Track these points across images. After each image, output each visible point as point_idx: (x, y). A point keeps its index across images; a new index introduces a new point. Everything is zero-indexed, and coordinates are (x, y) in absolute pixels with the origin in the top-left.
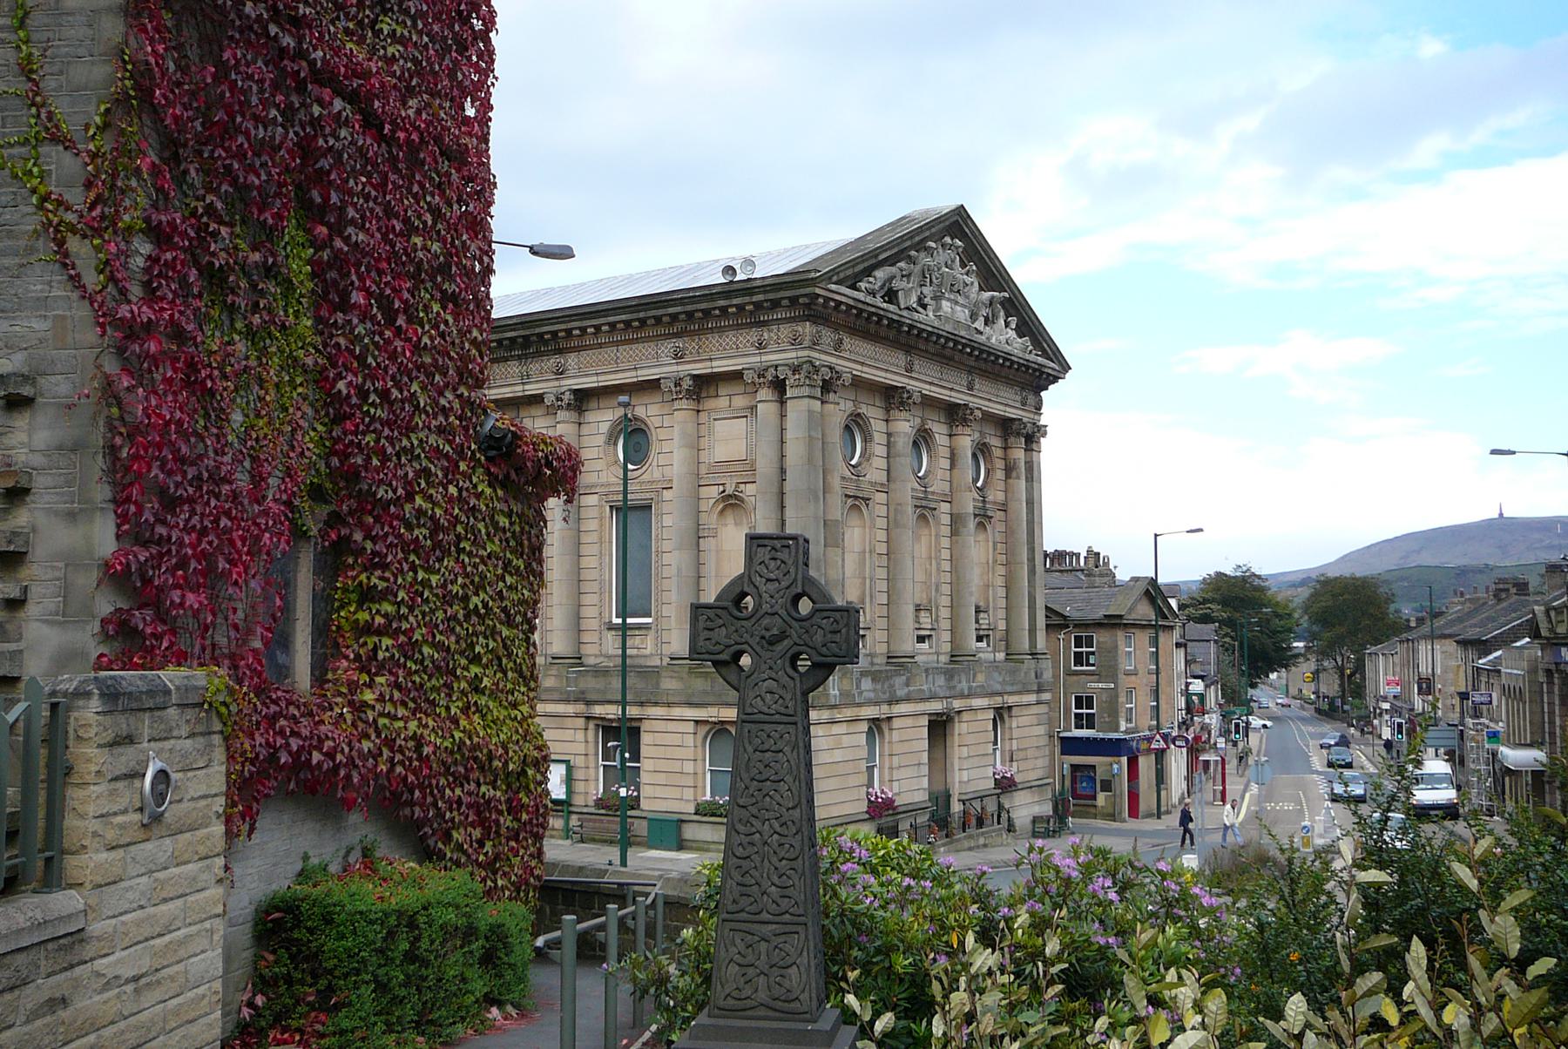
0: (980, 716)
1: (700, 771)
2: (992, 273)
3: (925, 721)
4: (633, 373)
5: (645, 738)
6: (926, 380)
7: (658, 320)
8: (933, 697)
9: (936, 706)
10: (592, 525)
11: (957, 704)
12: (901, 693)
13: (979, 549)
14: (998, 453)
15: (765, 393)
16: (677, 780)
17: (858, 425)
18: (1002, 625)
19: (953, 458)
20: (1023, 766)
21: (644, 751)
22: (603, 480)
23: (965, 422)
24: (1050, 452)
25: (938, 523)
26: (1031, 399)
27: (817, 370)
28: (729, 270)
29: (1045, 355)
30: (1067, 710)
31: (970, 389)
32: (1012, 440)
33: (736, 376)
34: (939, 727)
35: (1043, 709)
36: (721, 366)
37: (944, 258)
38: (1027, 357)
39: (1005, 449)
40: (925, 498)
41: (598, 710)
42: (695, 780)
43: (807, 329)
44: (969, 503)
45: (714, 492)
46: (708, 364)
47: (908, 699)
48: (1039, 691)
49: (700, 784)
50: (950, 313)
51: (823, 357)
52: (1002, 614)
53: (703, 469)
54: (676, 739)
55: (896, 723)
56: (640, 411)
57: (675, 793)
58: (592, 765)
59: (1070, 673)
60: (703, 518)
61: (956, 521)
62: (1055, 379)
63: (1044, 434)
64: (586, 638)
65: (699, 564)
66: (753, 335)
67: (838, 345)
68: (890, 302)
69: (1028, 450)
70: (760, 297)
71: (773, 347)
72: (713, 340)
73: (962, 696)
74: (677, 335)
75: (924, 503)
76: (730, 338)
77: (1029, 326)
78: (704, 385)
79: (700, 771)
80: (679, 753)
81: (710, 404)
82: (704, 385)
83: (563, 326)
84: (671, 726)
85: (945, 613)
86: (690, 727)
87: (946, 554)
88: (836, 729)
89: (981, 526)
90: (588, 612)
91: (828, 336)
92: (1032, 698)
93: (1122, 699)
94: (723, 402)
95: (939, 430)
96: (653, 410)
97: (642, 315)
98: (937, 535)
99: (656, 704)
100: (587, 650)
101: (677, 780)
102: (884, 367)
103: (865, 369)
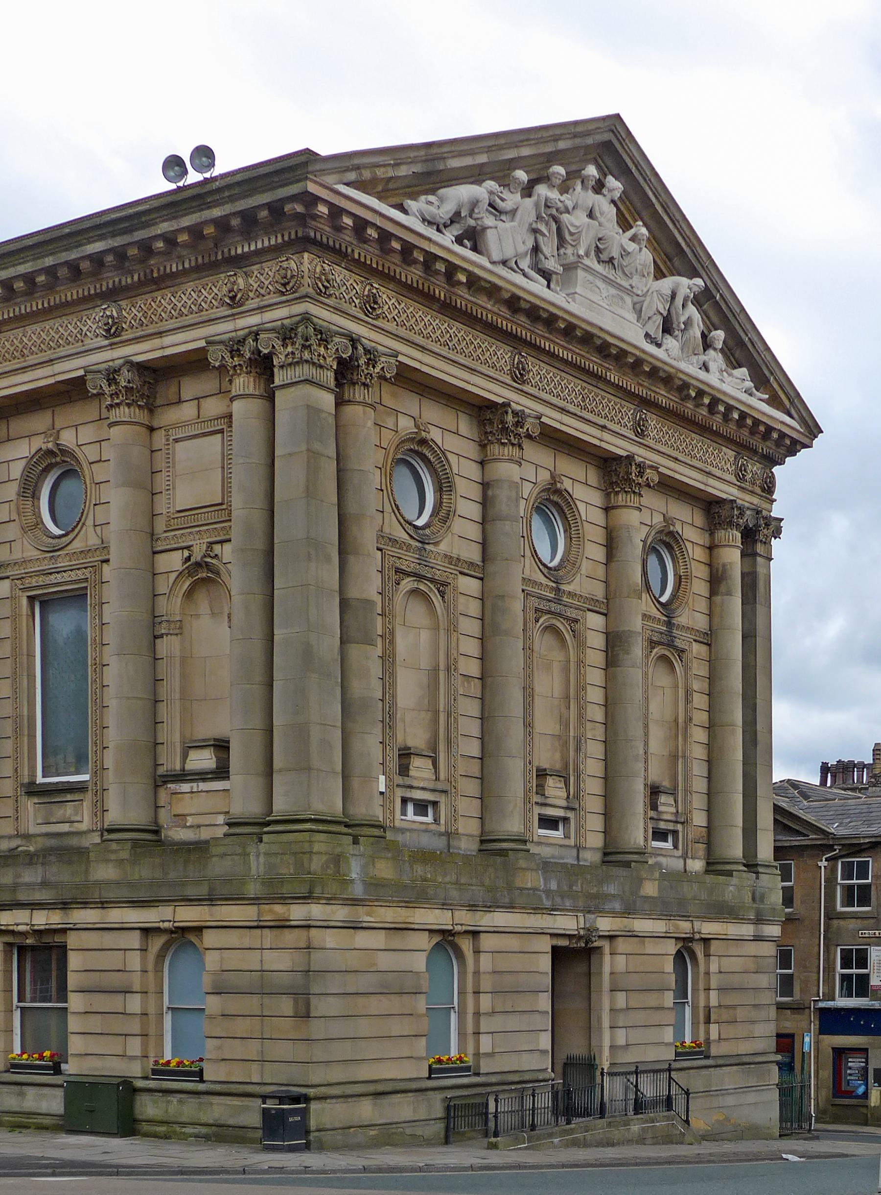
0: (651, 947)
1: (152, 1010)
2: (678, 249)
3: (545, 945)
5: (74, 961)
7: (75, 269)
9: (568, 923)
11: (605, 924)
13: (656, 697)
15: (243, 383)
16: (118, 1025)
18: (699, 819)
20: (729, 1031)
22: (17, 555)
25: (581, 644)
28: (173, 165)
29: (774, 401)
30: (830, 969)
31: (641, 434)
32: (721, 534)
33: (194, 363)
37: (590, 211)
40: (558, 601)
43: (307, 263)
44: (639, 614)
45: (174, 561)
46: (157, 342)
48: (759, 920)
49: (152, 1031)
53: (160, 525)
55: (487, 942)
56: (67, 439)
60: (162, 605)
61: (615, 644)
62: (794, 447)
63: (777, 533)
66: (219, 285)
69: (749, 554)
71: (251, 304)
74: (112, 295)
75: (554, 607)
77: (745, 348)
78: (156, 379)
84: (109, 940)
85: (593, 786)
86: (134, 940)
87: (595, 695)
88: (362, 939)
92: (747, 930)
94: (188, 411)
96: (87, 434)
97: (49, 261)
99: (85, 904)
101: (118, 1025)
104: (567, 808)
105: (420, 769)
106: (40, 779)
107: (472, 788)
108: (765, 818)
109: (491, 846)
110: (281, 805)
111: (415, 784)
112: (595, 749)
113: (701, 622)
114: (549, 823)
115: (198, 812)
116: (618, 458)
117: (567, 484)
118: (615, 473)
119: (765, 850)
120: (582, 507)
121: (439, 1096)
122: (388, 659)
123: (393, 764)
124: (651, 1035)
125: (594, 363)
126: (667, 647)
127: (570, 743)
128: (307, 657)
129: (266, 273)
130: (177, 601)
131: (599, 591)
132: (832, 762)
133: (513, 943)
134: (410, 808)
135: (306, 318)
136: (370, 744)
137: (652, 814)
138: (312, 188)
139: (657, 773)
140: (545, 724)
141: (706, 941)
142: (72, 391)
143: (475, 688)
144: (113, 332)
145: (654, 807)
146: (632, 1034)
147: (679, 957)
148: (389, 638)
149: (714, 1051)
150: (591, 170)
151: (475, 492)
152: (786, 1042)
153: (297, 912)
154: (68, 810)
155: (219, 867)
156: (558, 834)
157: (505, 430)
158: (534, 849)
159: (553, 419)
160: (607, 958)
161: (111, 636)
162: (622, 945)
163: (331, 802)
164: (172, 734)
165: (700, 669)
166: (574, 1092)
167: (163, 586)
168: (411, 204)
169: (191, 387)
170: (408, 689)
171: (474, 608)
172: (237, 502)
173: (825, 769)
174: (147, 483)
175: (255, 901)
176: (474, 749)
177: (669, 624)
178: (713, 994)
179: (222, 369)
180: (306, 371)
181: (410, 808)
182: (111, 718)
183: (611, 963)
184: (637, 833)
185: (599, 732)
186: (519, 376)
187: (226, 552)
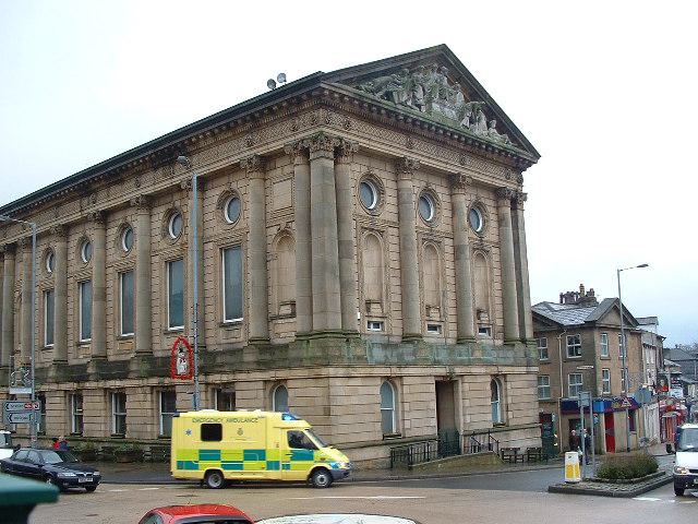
0: (480, 379)
2: (474, 91)
5: (291, 393)
6: (423, 154)
8: (436, 363)
9: (441, 371)
11: (458, 370)
12: (410, 359)
15: (298, 160)
17: (372, 181)
18: (499, 323)
19: (454, 209)
20: (517, 414)
23: (460, 186)
24: (529, 210)
25: (443, 252)
28: (271, 83)
29: (520, 146)
33: (280, 154)
34: (446, 388)
36: (275, 146)
39: (497, 208)
43: (321, 113)
44: (467, 237)
45: (274, 230)
47: (415, 364)
51: (335, 133)
52: (499, 314)
53: (269, 217)
54: (253, 394)
55: (406, 380)
56: (234, 186)
59: (566, 361)
60: (269, 248)
61: (457, 251)
63: (525, 199)
64: (209, 333)
65: (266, 280)
66: (289, 124)
67: (347, 126)
70: (289, 97)
71: (302, 129)
72: (269, 132)
73: (462, 364)
75: (431, 237)
76: (278, 128)
78: (265, 163)
81: (272, 174)
82: (265, 163)
84: (251, 385)
85: (451, 311)
86: (261, 385)
87: (450, 272)
88: (353, 382)
89: (481, 257)
90: (210, 317)
92: (523, 369)
93: (599, 375)
94: (279, 171)
95: (442, 192)
96: (241, 183)
100: (210, 341)
103: (372, 143)
105: (376, 310)
106: (225, 321)
107: (397, 315)
108: (528, 320)
109: (408, 338)
110: (316, 327)
112: (451, 296)
113: (495, 238)
114: (433, 328)
115: (285, 332)
116: (454, 175)
118: (453, 181)
119: (529, 334)
120: (440, 196)
121: (388, 448)
122: (360, 263)
123: (363, 307)
124: (483, 417)
126: (481, 252)
128: (324, 266)
129: (307, 118)
130: (275, 246)
131: (449, 229)
132: (565, 293)
133: (418, 380)
135: (322, 132)
136: (354, 301)
137: (478, 321)
138: (322, 85)
139: (479, 303)
140: (429, 285)
141: (505, 375)
142: (235, 168)
143: (397, 273)
144: (250, 144)
146: (474, 412)
147: (494, 385)
148: (360, 255)
149: (511, 423)
150: (436, 65)
151: (394, 193)
152: (545, 418)
153: (324, 371)
154: (235, 333)
155: (293, 354)
156: (436, 333)
157: (405, 168)
158: (425, 340)
159: (425, 161)
160: (460, 385)
161: (250, 261)
162: (466, 379)
163: (335, 323)
164: (274, 299)
165: (496, 258)
166: (448, 444)
167: (270, 240)
170: (369, 276)
171: (396, 240)
172: (296, 205)
173: (562, 296)
174: (263, 201)
175: (308, 368)
176: (398, 299)
178: (509, 398)
179: (290, 155)
180: (322, 153)
182: (93, 323)
183: (463, 388)
184: (472, 330)
185: (452, 288)
186: (410, 146)
187: (293, 225)
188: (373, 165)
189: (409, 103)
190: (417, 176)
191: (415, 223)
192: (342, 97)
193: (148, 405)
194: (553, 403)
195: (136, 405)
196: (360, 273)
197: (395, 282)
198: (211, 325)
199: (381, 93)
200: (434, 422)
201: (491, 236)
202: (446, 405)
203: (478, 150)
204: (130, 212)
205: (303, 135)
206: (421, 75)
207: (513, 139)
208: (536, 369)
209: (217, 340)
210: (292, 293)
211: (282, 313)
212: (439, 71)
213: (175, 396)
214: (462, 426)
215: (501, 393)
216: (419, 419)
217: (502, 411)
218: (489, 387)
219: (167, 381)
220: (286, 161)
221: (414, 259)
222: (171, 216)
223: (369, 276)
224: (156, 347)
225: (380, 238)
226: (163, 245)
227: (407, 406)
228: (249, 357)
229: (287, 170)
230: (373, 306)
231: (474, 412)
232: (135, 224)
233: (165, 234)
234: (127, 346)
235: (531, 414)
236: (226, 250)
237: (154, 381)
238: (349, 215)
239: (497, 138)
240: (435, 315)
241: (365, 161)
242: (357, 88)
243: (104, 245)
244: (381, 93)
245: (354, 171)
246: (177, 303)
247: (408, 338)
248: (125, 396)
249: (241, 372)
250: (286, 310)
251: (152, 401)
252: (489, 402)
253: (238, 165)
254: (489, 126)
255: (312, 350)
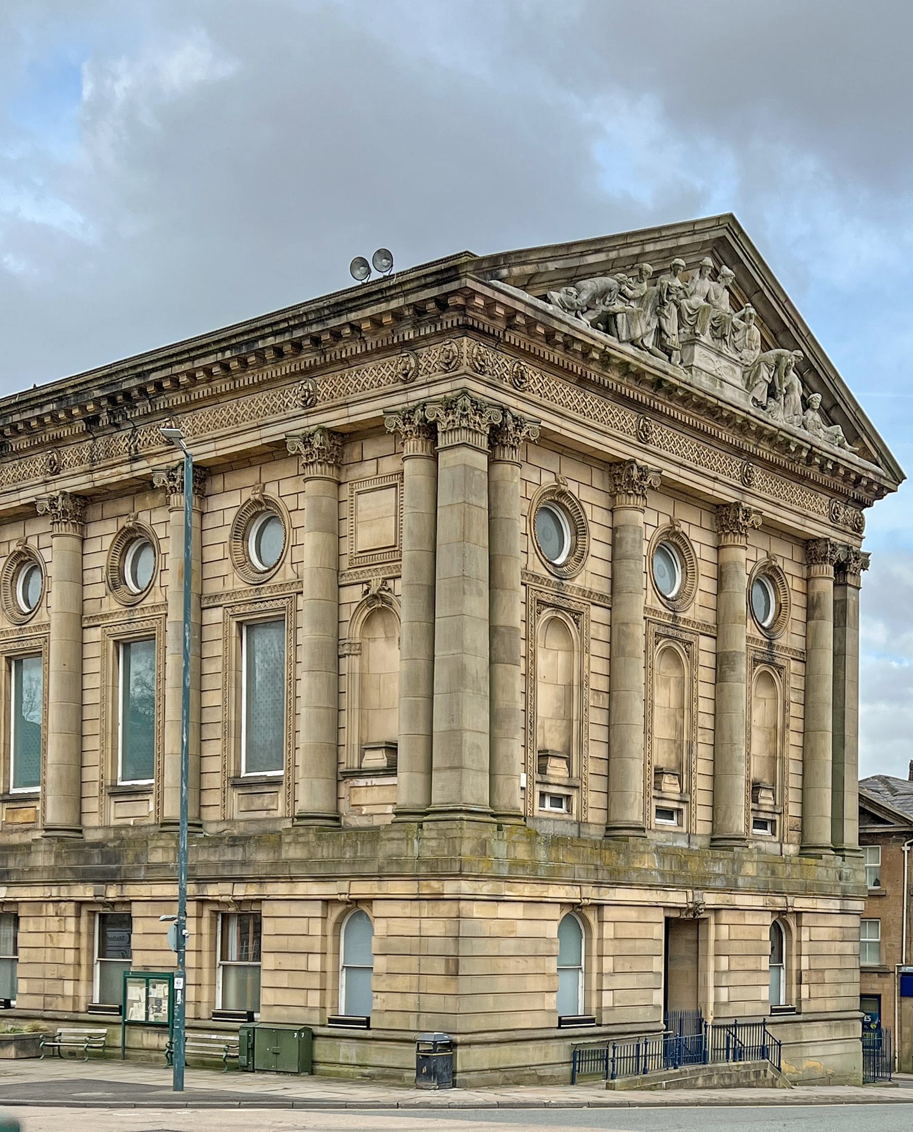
0: (750, 919)
1: (329, 968)
2: (782, 327)
3: (659, 916)
4: (256, 435)
5: (268, 926)
6: (669, 455)
10: (217, 649)
11: (710, 899)
13: (756, 709)
14: (796, 584)
15: (414, 445)
16: (301, 980)
19: (721, 578)
20: (817, 991)
21: (266, 942)
22: (229, 588)
26: (847, 513)
27: (479, 410)
29: (864, 453)
32: (816, 569)
33: (372, 430)
34: (683, 927)
35: (854, 921)
36: (364, 412)
38: (837, 450)
40: (675, 627)
41: (212, 891)
42: (323, 980)
43: (467, 346)
44: (743, 636)
45: (354, 594)
48: (845, 897)
50: (719, 371)
53: (345, 563)
55: (609, 913)
56: (272, 491)
57: (296, 998)
58: (206, 964)
61: (723, 663)
63: (865, 566)
68: (607, 331)
75: (671, 632)
78: (342, 444)
79: (329, 968)
80: (302, 944)
82: (341, 445)
83: (167, 372)
85: (702, 783)
86: (316, 910)
87: (705, 706)
88: (504, 910)
90: (212, 765)
91: (504, 363)
92: (834, 905)
94: (369, 469)
98: (692, 679)
101: (301, 980)
102: (608, 431)
104: (680, 801)
105: (557, 769)
108: (851, 807)
109: (613, 831)
111: (552, 780)
113: (797, 643)
114: (666, 813)
117: (684, 527)
119: (851, 835)
120: (696, 546)
122: (530, 676)
123: (534, 764)
125: (706, 424)
127: (683, 748)
133: (632, 914)
134: (548, 801)
135: (465, 392)
136: (515, 750)
137: (755, 806)
138: (470, 284)
139: (757, 771)
140: (662, 729)
141: (798, 914)
142: (276, 452)
143: (603, 701)
145: (755, 800)
147: (777, 931)
148: (531, 658)
150: (708, 261)
151: (606, 536)
152: (870, 1000)
153: (449, 888)
154: (266, 800)
156: (671, 824)
157: (631, 483)
159: (672, 472)
160: (712, 928)
161: (303, 656)
162: (725, 917)
163: (475, 791)
164: (351, 737)
165: (796, 683)
167: (346, 615)
168: (555, 296)
169: (371, 449)
170: (547, 700)
172: (406, 544)
174: (334, 527)
177: (770, 645)
181: (548, 801)
183: (718, 932)
184: (739, 821)
187: (398, 586)
188: (566, 472)
189: (649, 342)
190: (654, 500)
191: (642, 602)
192: (512, 314)
193: (68, 940)
194: (882, 972)
195: (39, 940)
196: (530, 693)
197: (597, 717)
198: (214, 781)
199: (592, 315)
200: (658, 997)
201: (791, 638)
202: (683, 967)
203: (794, 463)
204: (40, 526)
205: (422, 393)
206: (677, 282)
207: (853, 436)
208: (858, 905)
209: (103, 817)
210: (392, 725)
211: (366, 764)
212: (715, 275)
213: (130, 924)
214: (711, 1007)
215: (789, 947)
216: (633, 995)
217: (788, 984)
218: (766, 936)
219: (112, 892)
220: (385, 445)
221: (636, 676)
222: (131, 541)
223: (547, 700)
224: (91, 820)
225: (572, 627)
226: (111, 605)
227: (608, 964)
228: (41, 859)
229: (389, 466)
230: (553, 762)
231: (736, 986)
232: (47, 555)
233: (115, 583)
234: (24, 815)
235: (841, 995)
236: (248, 626)
237: (85, 892)
238: (513, 575)
239: (824, 437)
240: (670, 786)
241: (552, 462)
242: (545, 298)
243: (78, 576)
244: (592, 315)
245: (527, 480)
246: (141, 720)
247: (613, 831)
248: (126, 921)
249: (277, 879)
250: (377, 759)
251: (78, 933)
252: (765, 963)
253: (280, 445)
254: (806, 405)
255: (428, 844)
